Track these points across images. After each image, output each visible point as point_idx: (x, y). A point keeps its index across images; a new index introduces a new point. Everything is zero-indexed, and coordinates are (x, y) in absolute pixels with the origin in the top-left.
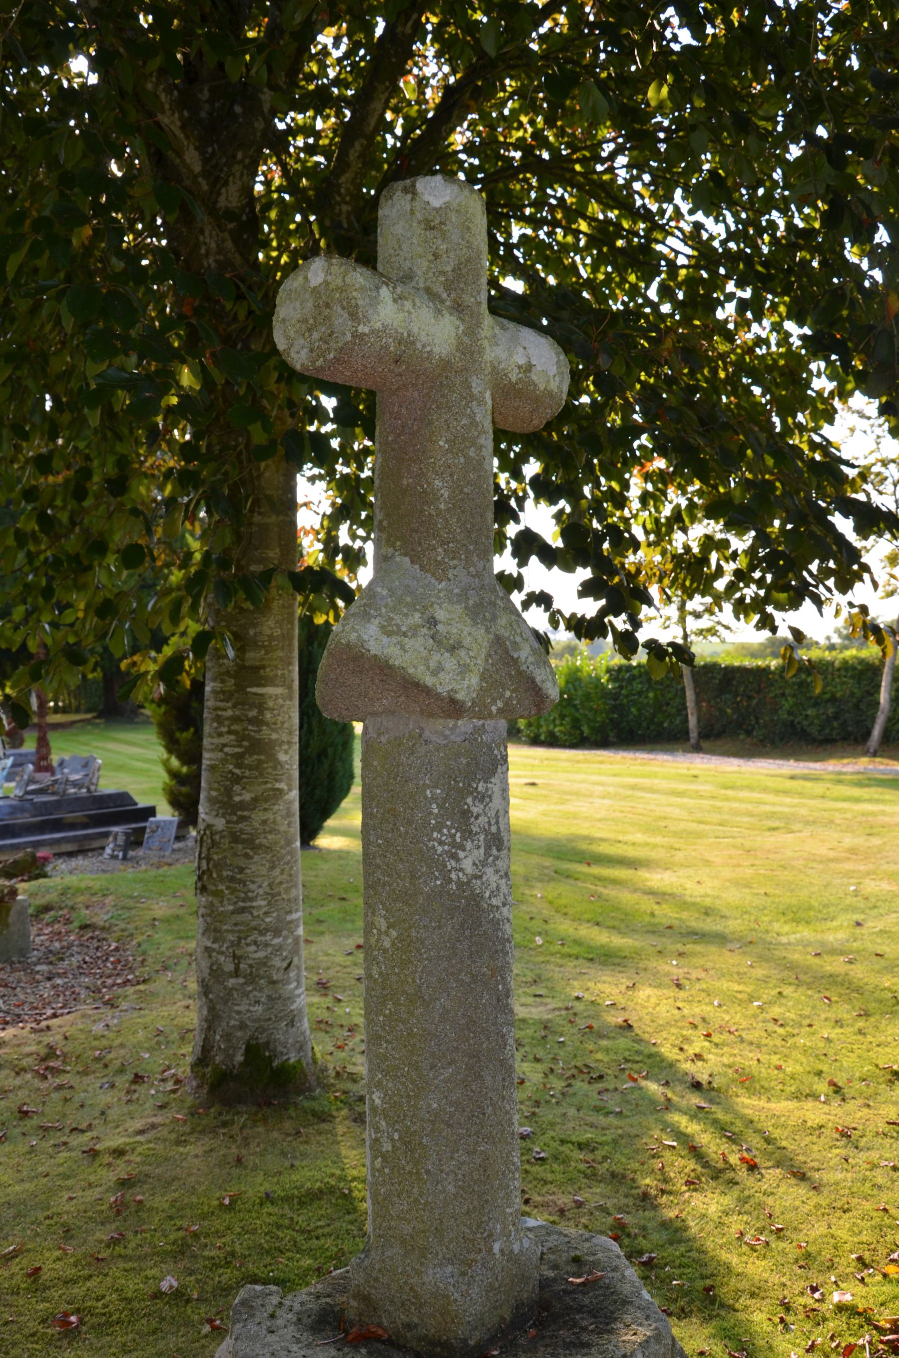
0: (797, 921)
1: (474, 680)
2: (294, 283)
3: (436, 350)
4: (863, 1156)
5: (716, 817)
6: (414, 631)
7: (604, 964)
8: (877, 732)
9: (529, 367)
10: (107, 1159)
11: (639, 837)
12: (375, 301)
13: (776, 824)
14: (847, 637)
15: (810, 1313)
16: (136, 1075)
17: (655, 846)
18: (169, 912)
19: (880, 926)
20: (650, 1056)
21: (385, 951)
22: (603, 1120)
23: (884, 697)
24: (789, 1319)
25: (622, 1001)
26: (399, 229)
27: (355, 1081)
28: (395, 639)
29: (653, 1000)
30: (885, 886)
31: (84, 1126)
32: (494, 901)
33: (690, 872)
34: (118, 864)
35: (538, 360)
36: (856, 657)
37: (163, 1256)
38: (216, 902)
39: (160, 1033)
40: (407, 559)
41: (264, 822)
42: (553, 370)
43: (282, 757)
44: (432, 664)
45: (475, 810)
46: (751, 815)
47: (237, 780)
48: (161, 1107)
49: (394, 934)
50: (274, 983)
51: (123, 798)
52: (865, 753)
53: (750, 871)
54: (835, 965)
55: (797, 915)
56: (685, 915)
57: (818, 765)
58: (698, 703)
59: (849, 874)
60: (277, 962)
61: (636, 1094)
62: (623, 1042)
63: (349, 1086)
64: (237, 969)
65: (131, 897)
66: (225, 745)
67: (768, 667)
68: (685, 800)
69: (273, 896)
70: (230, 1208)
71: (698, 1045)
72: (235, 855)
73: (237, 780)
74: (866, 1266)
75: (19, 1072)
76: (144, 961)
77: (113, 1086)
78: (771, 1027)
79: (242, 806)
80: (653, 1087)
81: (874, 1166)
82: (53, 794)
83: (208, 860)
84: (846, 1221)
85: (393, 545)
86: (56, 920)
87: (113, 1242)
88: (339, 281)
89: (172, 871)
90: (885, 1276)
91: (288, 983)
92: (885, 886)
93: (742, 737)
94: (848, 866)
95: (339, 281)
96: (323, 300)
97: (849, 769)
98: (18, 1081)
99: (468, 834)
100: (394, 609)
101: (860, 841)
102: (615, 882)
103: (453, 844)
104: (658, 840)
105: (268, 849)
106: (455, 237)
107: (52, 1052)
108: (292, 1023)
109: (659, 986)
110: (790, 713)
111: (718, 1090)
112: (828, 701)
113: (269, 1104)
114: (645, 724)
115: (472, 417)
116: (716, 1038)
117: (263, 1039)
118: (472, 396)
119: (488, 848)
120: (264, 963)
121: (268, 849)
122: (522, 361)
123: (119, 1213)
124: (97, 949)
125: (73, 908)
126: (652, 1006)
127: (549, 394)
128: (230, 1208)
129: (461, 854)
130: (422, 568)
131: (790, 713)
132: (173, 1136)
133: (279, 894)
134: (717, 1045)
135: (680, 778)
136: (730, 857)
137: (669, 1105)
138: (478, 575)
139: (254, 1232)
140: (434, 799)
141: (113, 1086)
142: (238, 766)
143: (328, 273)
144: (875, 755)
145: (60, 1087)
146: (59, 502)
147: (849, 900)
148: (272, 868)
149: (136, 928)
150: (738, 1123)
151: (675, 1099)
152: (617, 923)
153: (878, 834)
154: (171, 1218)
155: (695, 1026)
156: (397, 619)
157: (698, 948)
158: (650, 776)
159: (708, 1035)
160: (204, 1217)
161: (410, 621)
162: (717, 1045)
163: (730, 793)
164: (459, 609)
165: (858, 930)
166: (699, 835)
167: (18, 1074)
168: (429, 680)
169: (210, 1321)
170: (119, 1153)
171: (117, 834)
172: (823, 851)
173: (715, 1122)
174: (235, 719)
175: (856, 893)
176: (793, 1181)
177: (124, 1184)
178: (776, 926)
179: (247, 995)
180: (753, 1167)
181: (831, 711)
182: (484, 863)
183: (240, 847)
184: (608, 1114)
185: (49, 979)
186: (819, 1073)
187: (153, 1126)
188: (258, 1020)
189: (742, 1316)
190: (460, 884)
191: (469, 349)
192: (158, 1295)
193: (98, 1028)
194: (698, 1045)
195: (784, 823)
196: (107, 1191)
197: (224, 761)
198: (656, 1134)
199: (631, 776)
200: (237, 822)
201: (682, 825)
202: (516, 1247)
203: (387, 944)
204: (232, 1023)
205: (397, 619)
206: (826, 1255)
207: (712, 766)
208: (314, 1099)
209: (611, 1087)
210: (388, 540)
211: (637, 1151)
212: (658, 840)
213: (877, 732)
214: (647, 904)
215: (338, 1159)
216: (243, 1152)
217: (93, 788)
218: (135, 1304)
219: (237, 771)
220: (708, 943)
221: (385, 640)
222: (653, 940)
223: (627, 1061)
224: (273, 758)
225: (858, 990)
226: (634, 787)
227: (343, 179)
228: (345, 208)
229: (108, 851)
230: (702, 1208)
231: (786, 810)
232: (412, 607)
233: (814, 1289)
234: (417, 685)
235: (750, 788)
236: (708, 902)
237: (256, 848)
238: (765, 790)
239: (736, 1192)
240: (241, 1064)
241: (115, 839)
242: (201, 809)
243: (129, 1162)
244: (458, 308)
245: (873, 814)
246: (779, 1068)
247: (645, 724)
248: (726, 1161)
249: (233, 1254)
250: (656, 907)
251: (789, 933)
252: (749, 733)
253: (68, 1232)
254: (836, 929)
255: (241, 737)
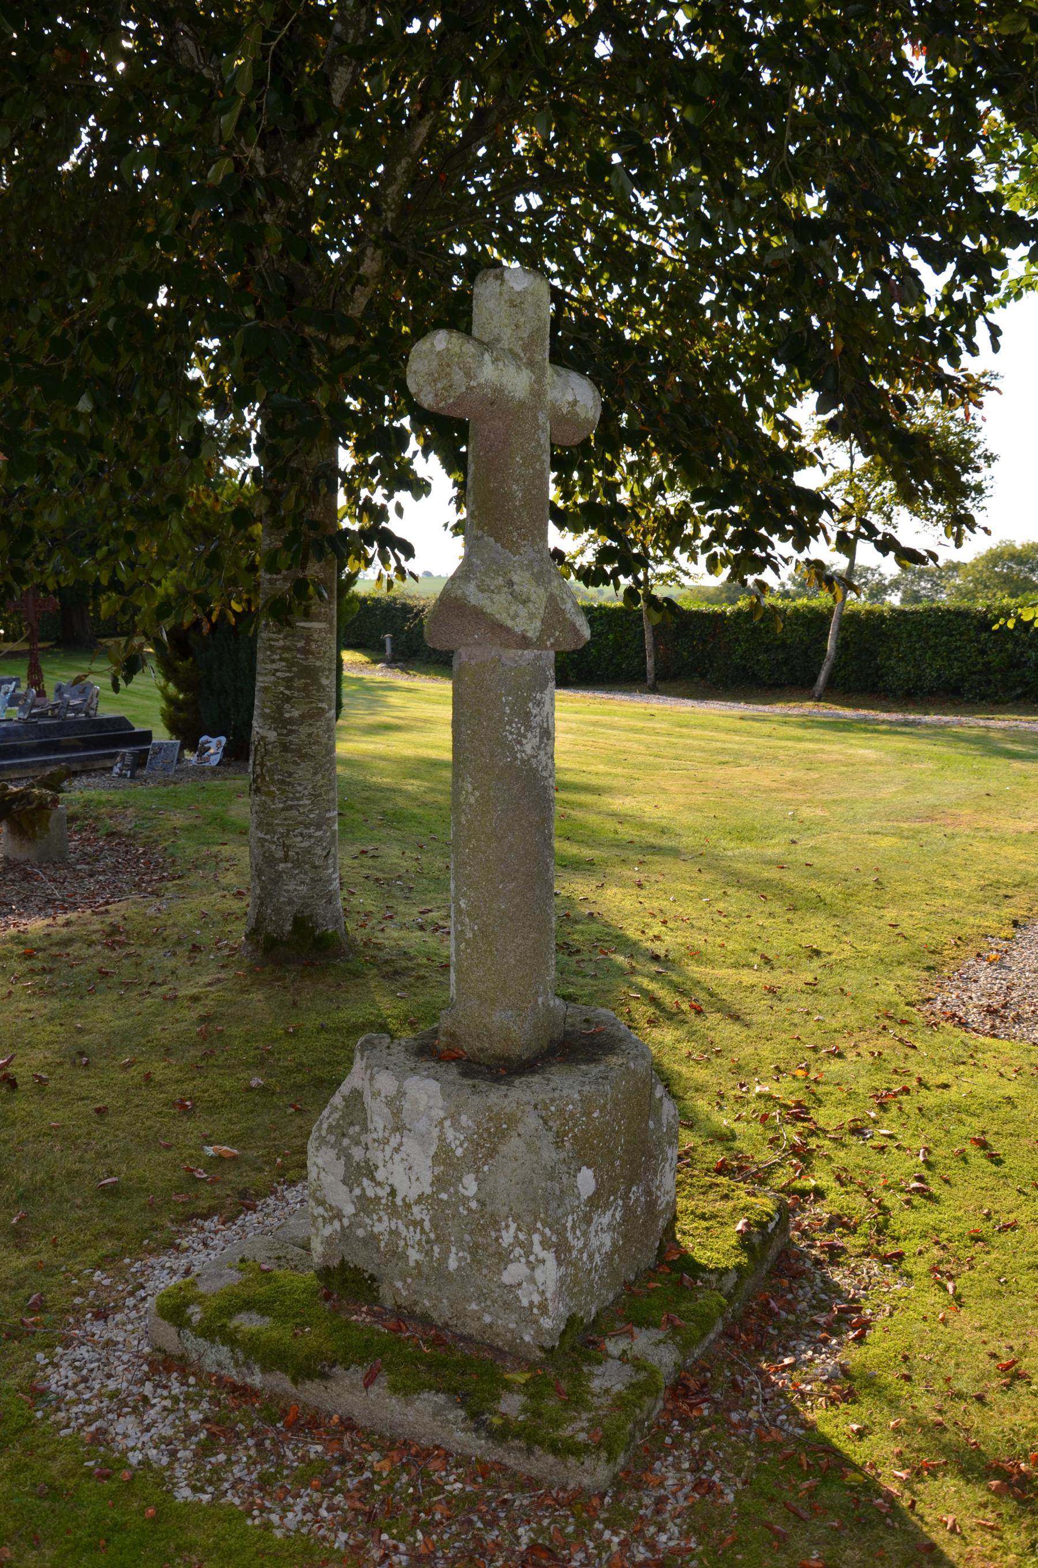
0: (741, 839)
1: (538, 623)
2: (422, 346)
3: (517, 395)
4: (784, 1005)
5: (672, 752)
6: (499, 589)
7: (576, 869)
8: (822, 678)
9: (575, 403)
10: (186, 1003)
11: (601, 768)
12: (481, 364)
13: (726, 759)
14: (801, 585)
15: (738, 1099)
16: (194, 946)
17: (616, 776)
18: (187, 822)
19: (812, 843)
20: (618, 937)
21: (471, 805)
22: (581, 981)
23: (830, 644)
24: (723, 1103)
25: (592, 897)
26: (491, 305)
27: (379, 949)
28: (486, 595)
29: (619, 896)
30: (819, 812)
31: (160, 981)
32: (544, 774)
33: (648, 798)
34: (126, 782)
35: (579, 396)
36: (806, 606)
37: (247, 1065)
38: (269, 802)
39: (205, 915)
40: (492, 540)
41: (310, 735)
42: (591, 403)
43: (324, 681)
44: (512, 613)
45: (534, 712)
46: (703, 750)
47: (288, 699)
48: (223, 967)
49: (477, 794)
50: (316, 867)
51: (121, 723)
52: (810, 698)
53: (701, 799)
54: (772, 873)
55: (741, 834)
56: (644, 833)
57: (766, 708)
58: (655, 646)
59: (788, 802)
60: (319, 851)
61: (607, 963)
62: (594, 927)
63: (376, 952)
64: (286, 856)
65: (150, 809)
66: (277, 670)
67: (724, 613)
68: (643, 736)
69: (316, 796)
70: (294, 1035)
71: (657, 929)
72: (286, 762)
73: (288, 699)
74: (781, 1072)
75: (91, 944)
76: (174, 862)
77: (174, 954)
78: (717, 917)
79: (290, 721)
80: (620, 959)
81: (793, 1012)
82: (54, 717)
83: (262, 765)
84: (768, 1046)
85: (482, 529)
86: (82, 829)
87: (204, 1057)
88: (457, 349)
89: (179, 788)
90: (794, 1076)
91: (327, 869)
92: (819, 812)
93: (696, 679)
94: (788, 795)
95: (457, 349)
96: (445, 362)
97: (795, 712)
98: (91, 951)
99: (529, 728)
100: (485, 574)
101: (800, 775)
102: (581, 806)
103: (519, 734)
104: (619, 771)
105: (312, 757)
106: (530, 313)
107: (115, 929)
108: (329, 902)
109: (623, 886)
110: (742, 658)
111: (674, 961)
112: (778, 647)
113: (312, 965)
114: (604, 665)
115: (538, 441)
116: (670, 925)
117: (307, 912)
118: (539, 426)
119: (541, 738)
120: (308, 851)
121: (312, 757)
122: (570, 399)
123: (205, 1039)
124: (127, 852)
125: (97, 818)
126: (619, 902)
127: (587, 420)
128: (294, 1035)
129: (524, 741)
130: (503, 546)
131: (742, 658)
132: (238, 987)
133: (320, 795)
134: (672, 930)
135: (638, 716)
136: (684, 786)
137: (633, 971)
138: (539, 552)
139: (315, 1050)
140: (507, 703)
141: (174, 954)
142: (288, 688)
143: (449, 342)
144: (819, 700)
145: (128, 956)
146: (142, 461)
147: (787, 823)
148: (315, 774)
149: (160, 835)
150: (689, 983)
151: (638, 967)
152: (585, 838)
153: (816, 769)
154: (248, 1041)
155: (654, 916)
156: (488, 581)
157: (656, 858)
158: (609, 714)
159: (665, 922)
160: (274, 1041)
161: (496, 582)
162: (672, 930)
163: (684, 730)
164: (528, 574)
165: (793, 846)
166: (656, 767)
167: (90, 946)
168: (509, 623)
169: (292, 1106)
170: (195, 999)
171: (124, 754)
172: (767, 782)
173: (670, 982)
174: (286, 649)
175: (793, 817)
176: (729, 1021)
177: (203, 1019)
178: (723, 843)
179: (294, 876)
180: (699, 1012)
181: (781, 656)
182: (539, 748)
183: (289, 755)
184: (584, 976)
185: (91, 876)
186: (754, 950)
187: (219, 980)
188: (304, 897)
189: (688, 1103)
190: (523, 761)
191: (537, 393)
192: (249, 1089)
193: (151, 911)
194: (657, 929)
195: (735, 759)
196: (192, 1024)
197: (276, 684)
198: (625, 989)
199: (592, 713)
200: (287, 735)
201: (640, 759)
202: (552, 1003)
203: (472, 800)
204: (282, 899)
205: (488, 581)
206: (752, 1066)
207: (668, 706)
208: (348, 961)
209: (587, 958)
210: (478, 525)
211: (609, 1001)
212: (619, 771)
213: (822, 678)
214: (610, 825)
215: (373, 1003)
216: (297, 998)
217: (92, 712)
218: (233, 1095)
219: (287, 692)
220: (664, 855)
221: (480, 595)
222: (618, 852)
223: (598, 940)
224: (316, 681)
225: (790, 891)
226: (595, 724)
227: (389, 191)
228: (390, 215)
229: (116, 770)
230: (660, 1038)
231: (736, 746)
232: (497, 572)
233: (742, 1086)
234: (501, 626)
235: (702, 726)
236: (664, 822)
237: (304, 757)
238: (717, 729)
239: (686, 1027)
240: (289, 932)
241: (123, 759)
242: (255, 723)
243: (205, 1005)
244: (531, 364)
245: (814, 752)
246: (722, 946)
247: (604, 665)
248: (678, 1007)
249: (302, 1064)
250: (619, 826)
251: (731, 848)
252: (703, 676)
253: (168, 1051)
254: (774, 846)
255: (291, 664)
